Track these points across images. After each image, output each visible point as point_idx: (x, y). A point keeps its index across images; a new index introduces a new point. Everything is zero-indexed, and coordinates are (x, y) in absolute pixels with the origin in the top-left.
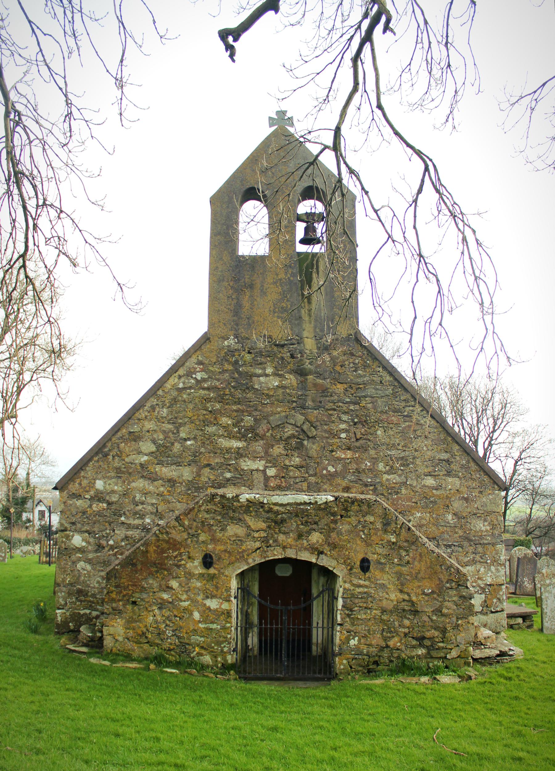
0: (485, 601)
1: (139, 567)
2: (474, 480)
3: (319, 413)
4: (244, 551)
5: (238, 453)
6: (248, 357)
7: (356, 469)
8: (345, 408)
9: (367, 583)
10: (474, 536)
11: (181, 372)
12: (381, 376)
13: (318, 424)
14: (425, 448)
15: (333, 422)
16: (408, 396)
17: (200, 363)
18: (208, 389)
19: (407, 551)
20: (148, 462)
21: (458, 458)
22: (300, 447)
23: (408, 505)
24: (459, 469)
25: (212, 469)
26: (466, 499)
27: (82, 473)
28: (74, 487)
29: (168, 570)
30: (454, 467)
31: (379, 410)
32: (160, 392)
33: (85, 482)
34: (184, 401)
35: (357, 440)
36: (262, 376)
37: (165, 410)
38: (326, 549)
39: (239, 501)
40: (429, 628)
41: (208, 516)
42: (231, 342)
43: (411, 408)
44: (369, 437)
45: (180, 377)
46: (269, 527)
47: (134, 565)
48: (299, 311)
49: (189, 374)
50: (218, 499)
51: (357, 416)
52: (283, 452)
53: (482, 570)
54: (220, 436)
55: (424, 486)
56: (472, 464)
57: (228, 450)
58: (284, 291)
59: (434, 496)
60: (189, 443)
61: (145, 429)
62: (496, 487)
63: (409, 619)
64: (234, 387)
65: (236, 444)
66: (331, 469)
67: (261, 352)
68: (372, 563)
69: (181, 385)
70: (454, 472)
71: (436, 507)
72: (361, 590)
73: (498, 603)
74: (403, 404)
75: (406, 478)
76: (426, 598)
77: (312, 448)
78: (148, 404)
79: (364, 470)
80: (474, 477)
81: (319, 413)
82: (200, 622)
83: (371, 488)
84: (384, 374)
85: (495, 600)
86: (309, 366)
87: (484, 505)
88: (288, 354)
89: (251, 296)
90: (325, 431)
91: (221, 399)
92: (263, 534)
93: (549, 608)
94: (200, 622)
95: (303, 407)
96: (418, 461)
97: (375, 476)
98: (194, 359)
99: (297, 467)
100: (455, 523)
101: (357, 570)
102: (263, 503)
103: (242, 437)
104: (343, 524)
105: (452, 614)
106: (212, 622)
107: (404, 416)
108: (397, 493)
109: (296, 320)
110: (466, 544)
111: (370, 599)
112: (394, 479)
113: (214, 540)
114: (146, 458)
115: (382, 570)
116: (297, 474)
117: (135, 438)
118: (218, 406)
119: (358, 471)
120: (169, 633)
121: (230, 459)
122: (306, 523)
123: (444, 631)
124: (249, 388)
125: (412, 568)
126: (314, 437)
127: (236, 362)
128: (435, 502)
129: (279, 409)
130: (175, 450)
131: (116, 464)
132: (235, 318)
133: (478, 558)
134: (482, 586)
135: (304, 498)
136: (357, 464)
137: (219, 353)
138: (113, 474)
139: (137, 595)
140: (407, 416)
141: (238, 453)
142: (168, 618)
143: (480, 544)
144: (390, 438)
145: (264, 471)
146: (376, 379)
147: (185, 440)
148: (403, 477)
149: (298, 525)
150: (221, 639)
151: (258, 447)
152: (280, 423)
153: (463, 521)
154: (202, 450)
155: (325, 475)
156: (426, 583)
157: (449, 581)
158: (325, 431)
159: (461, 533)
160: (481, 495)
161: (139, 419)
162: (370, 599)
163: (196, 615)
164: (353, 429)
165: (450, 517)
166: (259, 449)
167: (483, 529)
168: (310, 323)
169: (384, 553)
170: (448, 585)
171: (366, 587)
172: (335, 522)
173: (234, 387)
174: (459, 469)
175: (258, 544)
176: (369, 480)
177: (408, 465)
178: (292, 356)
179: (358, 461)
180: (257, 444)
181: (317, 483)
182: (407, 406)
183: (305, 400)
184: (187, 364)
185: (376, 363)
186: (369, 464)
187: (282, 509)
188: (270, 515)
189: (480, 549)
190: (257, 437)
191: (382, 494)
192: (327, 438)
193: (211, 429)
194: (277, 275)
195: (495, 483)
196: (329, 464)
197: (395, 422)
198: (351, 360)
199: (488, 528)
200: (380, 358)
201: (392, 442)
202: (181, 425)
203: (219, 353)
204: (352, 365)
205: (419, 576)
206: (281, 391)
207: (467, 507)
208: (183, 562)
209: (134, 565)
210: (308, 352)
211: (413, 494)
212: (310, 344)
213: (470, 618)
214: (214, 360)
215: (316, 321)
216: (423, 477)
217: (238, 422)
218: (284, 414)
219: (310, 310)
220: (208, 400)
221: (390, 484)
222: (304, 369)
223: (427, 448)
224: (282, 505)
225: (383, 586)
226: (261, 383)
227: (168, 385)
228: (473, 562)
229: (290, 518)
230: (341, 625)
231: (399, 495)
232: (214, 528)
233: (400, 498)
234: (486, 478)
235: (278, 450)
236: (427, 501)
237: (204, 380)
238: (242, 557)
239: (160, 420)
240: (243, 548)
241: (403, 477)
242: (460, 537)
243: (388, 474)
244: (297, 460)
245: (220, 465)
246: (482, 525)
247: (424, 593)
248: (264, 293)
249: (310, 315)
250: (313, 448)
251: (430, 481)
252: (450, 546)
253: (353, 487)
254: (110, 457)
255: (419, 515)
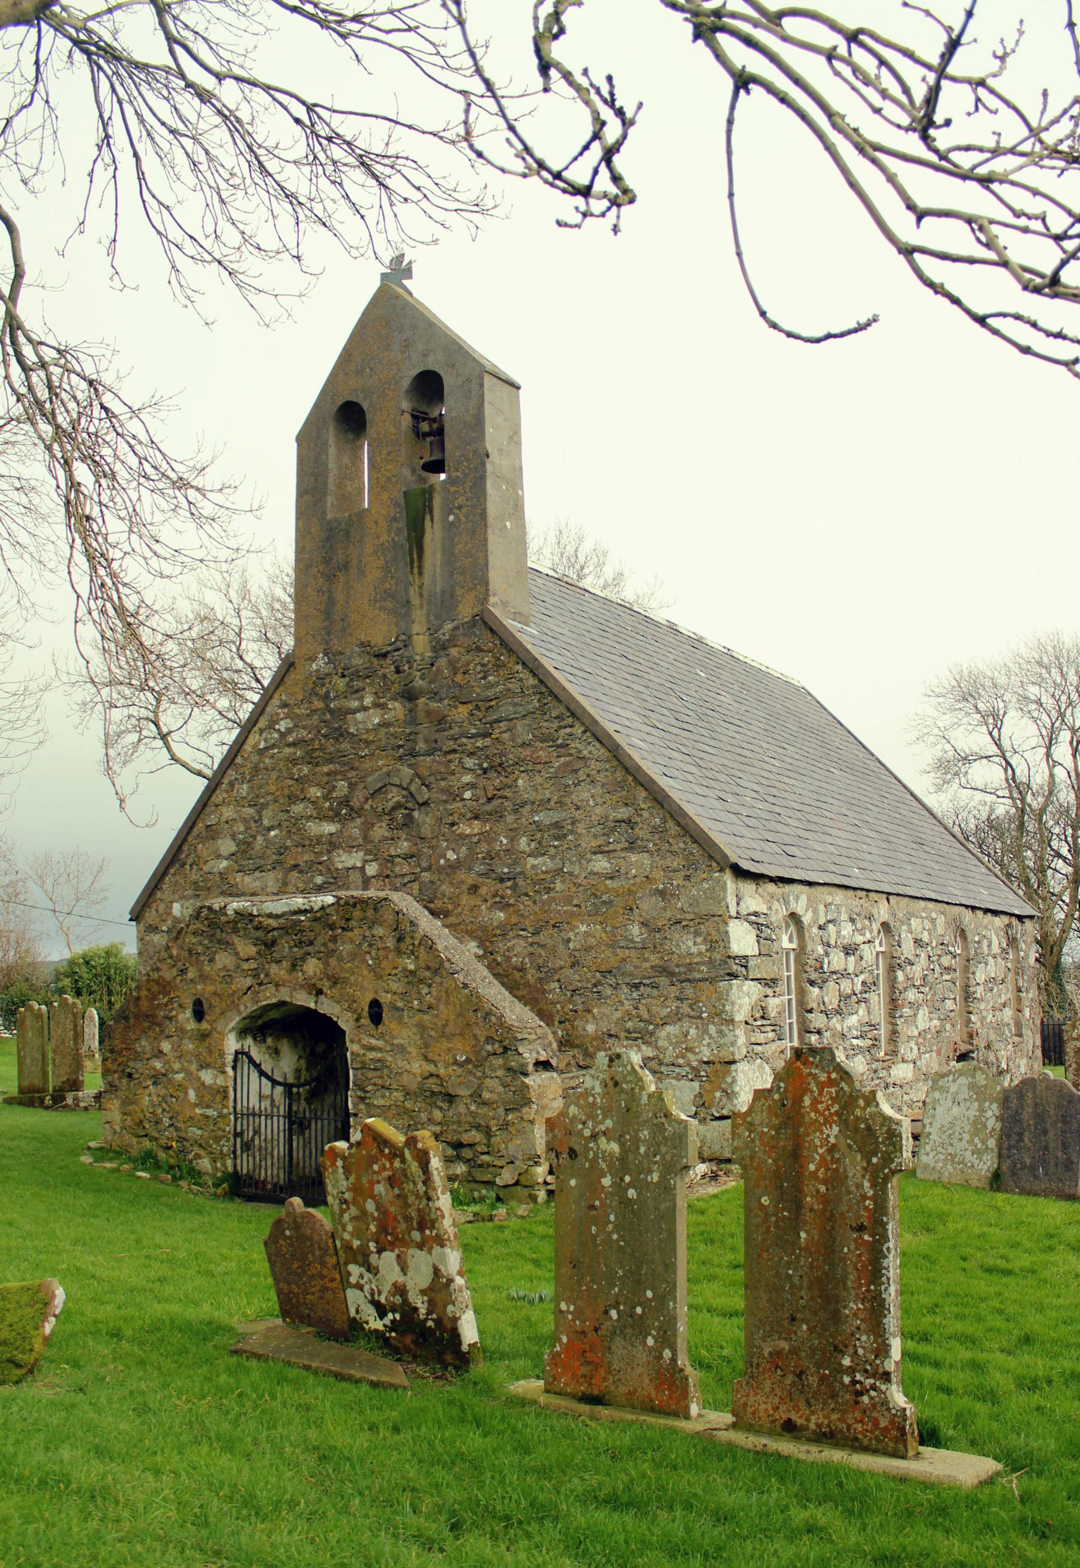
0: (700, 1095)
1: (132, 1021)
2: (674, 854)
3: (434, 761)
4: (234, 992)
5: (331, 843)
6: (341, 683)
7: (488, 853)
8: (469, 747)
9: (380, 1043)
10: (678, 966)
11: (262, 723)
12: (521, 680)
13: (432, 779)
14: (591, 803)
15: (453, 773)
16: (562, 709)
17: (284, 705)
18: (294, 744)
19: (430, 986)
20: (227, 868)
21: (646, 814)
22: (408, 822)
23: (566, 912)
24: (649, 836)
25: (301, 872)
26: (662, 893)
27: (159, 894)
28: (150, 916)
29: (160, 1025)
30: (641, 832)
31: (520, 741)
32: (239, 760)
33: (162, 907)
34: (266, 769)
35: (490, 800)
36: (358, 711)
37: (245, 786)
38: (325, 985)
39: (226, 915)
40: (467, 1127)
41: (194, 940)
42: (320, 664)
43: (568, 730)
44: (507, 792)
45: (261, 731)
46: (258, 953)
47: (127, 1018)
48: (407, 591)
49: (271, 726)
50: (205, 912)
51: (487, 757)
52: (386, 834)
53: (693, 1031)
54: (310, 818)
55: (592, 873)
56: (670, 824)
57: (319, 839)
58: (387, 562)
59: (608, 890)
60: (272, 833)
61: (224, 819)
62: (714, 864)
63: (441, 1108)
64: (325, 736)
65: (329, 828)
66: (451, 856)
67: (358, 671)
68: (385, 1009)
69: (262, 745)
70: (639, 842)
71: (611, 911)
72: (373, 1055)
73: (724, 1100)
74: (556, 725)
75: (562, 860)
76: (459, 1071)
77: (424, 823)
78: (226, 781)
79: (498, 853)
80: (675, 848)
81: (434, 761)
82: (196, 1105)
83: (509, 884)
84: (525, 675)
85: (718, 1094)
86: (420, 682)
87: (694, 902)
88: (392, 668)
89: (347, 582)
90: (442, 790)
91: (310, 759)
92: (253, 965)
93: (937, 1125)
94: (196, 1105)
95: (413, 754)
96: (581, 829)
97: (515, 863)
98: (275, 701)
99: (407, 857)
100: (643, 941)
101: (365, 1021)
102: (251, 915)
103: (334, 816)
104: (344, 943)
105: (496, 1102)
106: (208, 1107)
107: (558, 746)
108: (549, 890)
109: (402, 609)
110: (663, 981)
111: (386, 1071)
112: (544, 864)
113: (203, 977)
114: (225, 863)
115: (400, 1020)
116: (406, 869)
117: (213, 833)
118: (306, 770)
119: (490, 856)
120: (166, 1122)
121: (321, 853)
122: (300, 944)
123: (488, 1134)
124: (341, 734)
125: (436, 1016)
126: (425, 804)
127: (327, 696)
128: (610, 903)
129: (381, 763)
130: (258, 848)
131: (194, 877)
132: (327, 623)
133: (685, 1009)
134: (695, 1064)
135: (299, 902)
136: (489, 843)
137: (306, 684)
138: (190, 892)
139: (131, 1064)
140: (561, 746)
141: (331, 843)
142: (164, 1098)
143: (689, 980)
144: (536, 790)
145: (363, 868)
146: (514, 686)
147: (269, 829)
148: (557, 861)
149: (290, 948)
150: (221, 1133)
151: (354, 830)
152: (380, 785)
153: (658, 936)
154: (289, 843)
155: (443, 868)
156: (458, 1044)
157: (489, 1039)
158: (442, 790)
159: (654, 959)
160: (687, 884)
161: (217, 806)
162: (386, 1071)
163: (192, 1095)
164: (482, 782)
165: (635, 930)
166: (356, 832)
167: (694, 950)
168: (422, 608)
169: (400, 990)
170: (489, 1048)
171: (380, 1049)
172: (334, 939)
173: (325, 736)
174: (649, 836)
175: (249, 981)
176: (506, 870)
177: (565, 836)
178: (398, 671)
179: (488, 837)
180: (353, 825)
181: (432, 882)
182: (561, 727)
183: (415, 742)
184: (268, 709)
185: (513, 659)
186: (505, 841)
187: (273, 923)
188: (260, 934)
189: (689, 991)
190: (356, 812)
191: (526, 894)
192: (446, 802)
193: (298, 808)
194: (378, 537)
195: (711, 857)
196: (448, 848)
197: (544, 759)
198: (477, 660)
199: (703, 948)
200: (515, 648)
201: (539, 797)
202: (264, 806)
203: (306, 684)
204: (479, 668)
205: (448, 1030)
206: (383, 731)
207: (664, 909)
208: (174, 1013)
209: (127, 1018)
210: (418, 658)
211: (574, 889)
212: (421, 644)
213: (525, 1110)
214: (300, 697)
215: (430, 602)
216: (589, 856)
217: (330, 792)
218: (385, 769)
219: (421, 587)
220: (294, 762)
221: (537, 874)
222: (413, 688)
223: (593, 800)
224: (277, 917)
225: (402, 1049)
226: (357, 723)
227: (248, 747)
228: (677, 1017)
229: (281, 937)
230: (355, 1115)
231: (552, 894)
232: (202, 958)
233: (553, 899)
234: (695, 849)
235: (380, 831)
236: (599, 903)
237: (289, 731)
238: (234, 1006)
239: (239, 802)
240: (233, 987)
241: (557, 861)
242: (652, 967)
243: (535, 857)
244: (405, 846)
245: (311, 864)
246: (690, 944)
247: (456, 1063)
248: (362, 573)
249: (421, 595)
250: (425, 820)
251: (601, 864)
252: (636, 986)
253: (484, 884)
254: (188, 867)
255: (583, 928)
